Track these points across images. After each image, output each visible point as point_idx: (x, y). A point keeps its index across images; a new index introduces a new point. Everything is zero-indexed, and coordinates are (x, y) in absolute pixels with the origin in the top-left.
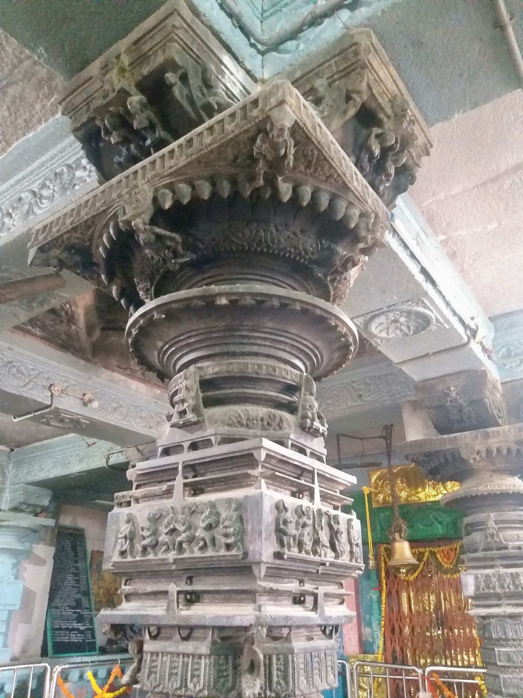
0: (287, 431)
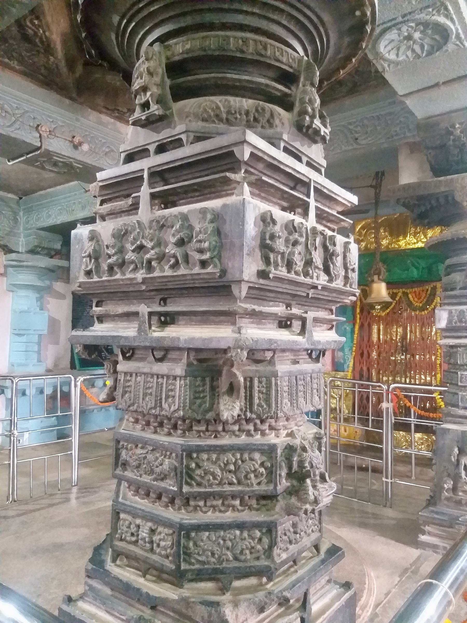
0: (279, 129)
